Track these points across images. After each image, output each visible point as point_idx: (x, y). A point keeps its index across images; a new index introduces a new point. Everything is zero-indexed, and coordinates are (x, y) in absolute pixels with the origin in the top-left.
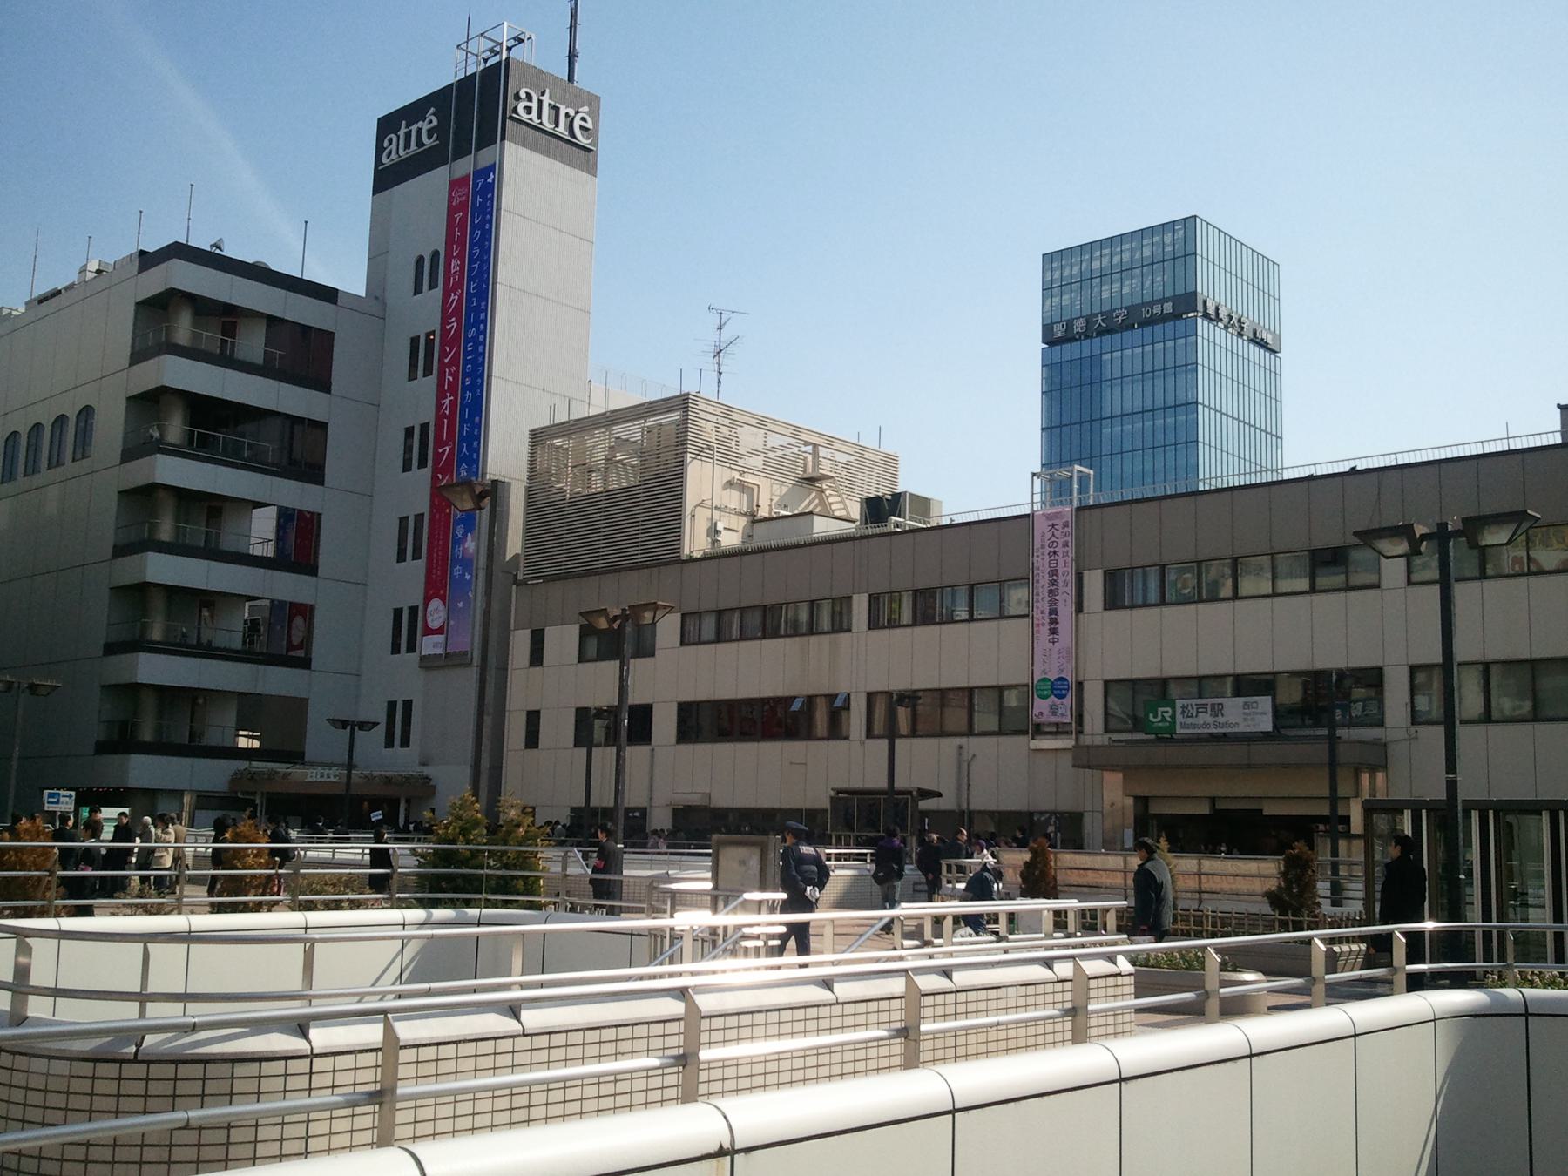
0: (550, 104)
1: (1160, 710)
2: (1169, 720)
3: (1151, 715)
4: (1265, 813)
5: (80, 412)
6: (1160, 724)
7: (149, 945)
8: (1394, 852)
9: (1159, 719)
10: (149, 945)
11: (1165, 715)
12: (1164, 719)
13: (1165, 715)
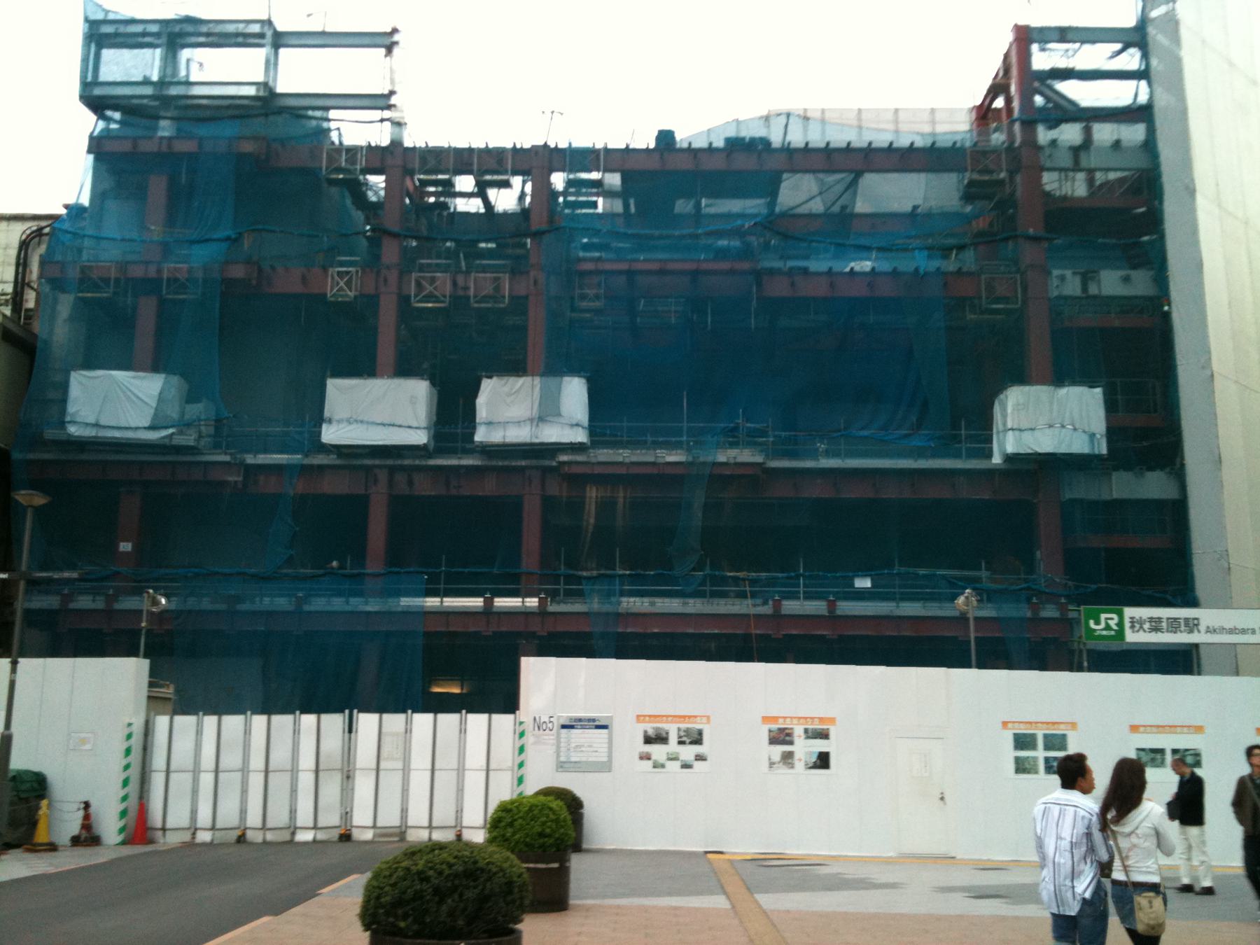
1: (1103, 616)
2: (1115, 628)
4: (85, 200)
9: (1103, 625)
11: (1110, 622)
12: (1108, 627)
13: (1110, 622)
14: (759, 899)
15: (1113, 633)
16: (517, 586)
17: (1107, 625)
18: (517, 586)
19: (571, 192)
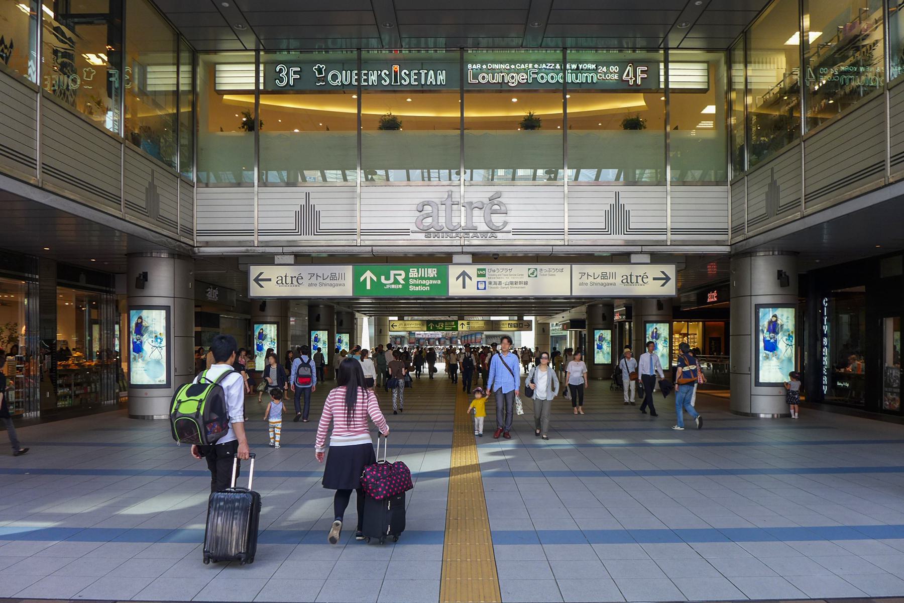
0: (789, 142)
1: (392, 273)
2: (402, 282)
3: (383, 278)
5: (218, 94)
6: (393, 286)
7: (410, 171)
8: (316, 351)
9: (392, 280)
10: (410, 171)
14: (699, 171)
15: (400, 286)
16: (669, 183)
17: (395, 279)
18: (669, 183)
19: (259, 66)
